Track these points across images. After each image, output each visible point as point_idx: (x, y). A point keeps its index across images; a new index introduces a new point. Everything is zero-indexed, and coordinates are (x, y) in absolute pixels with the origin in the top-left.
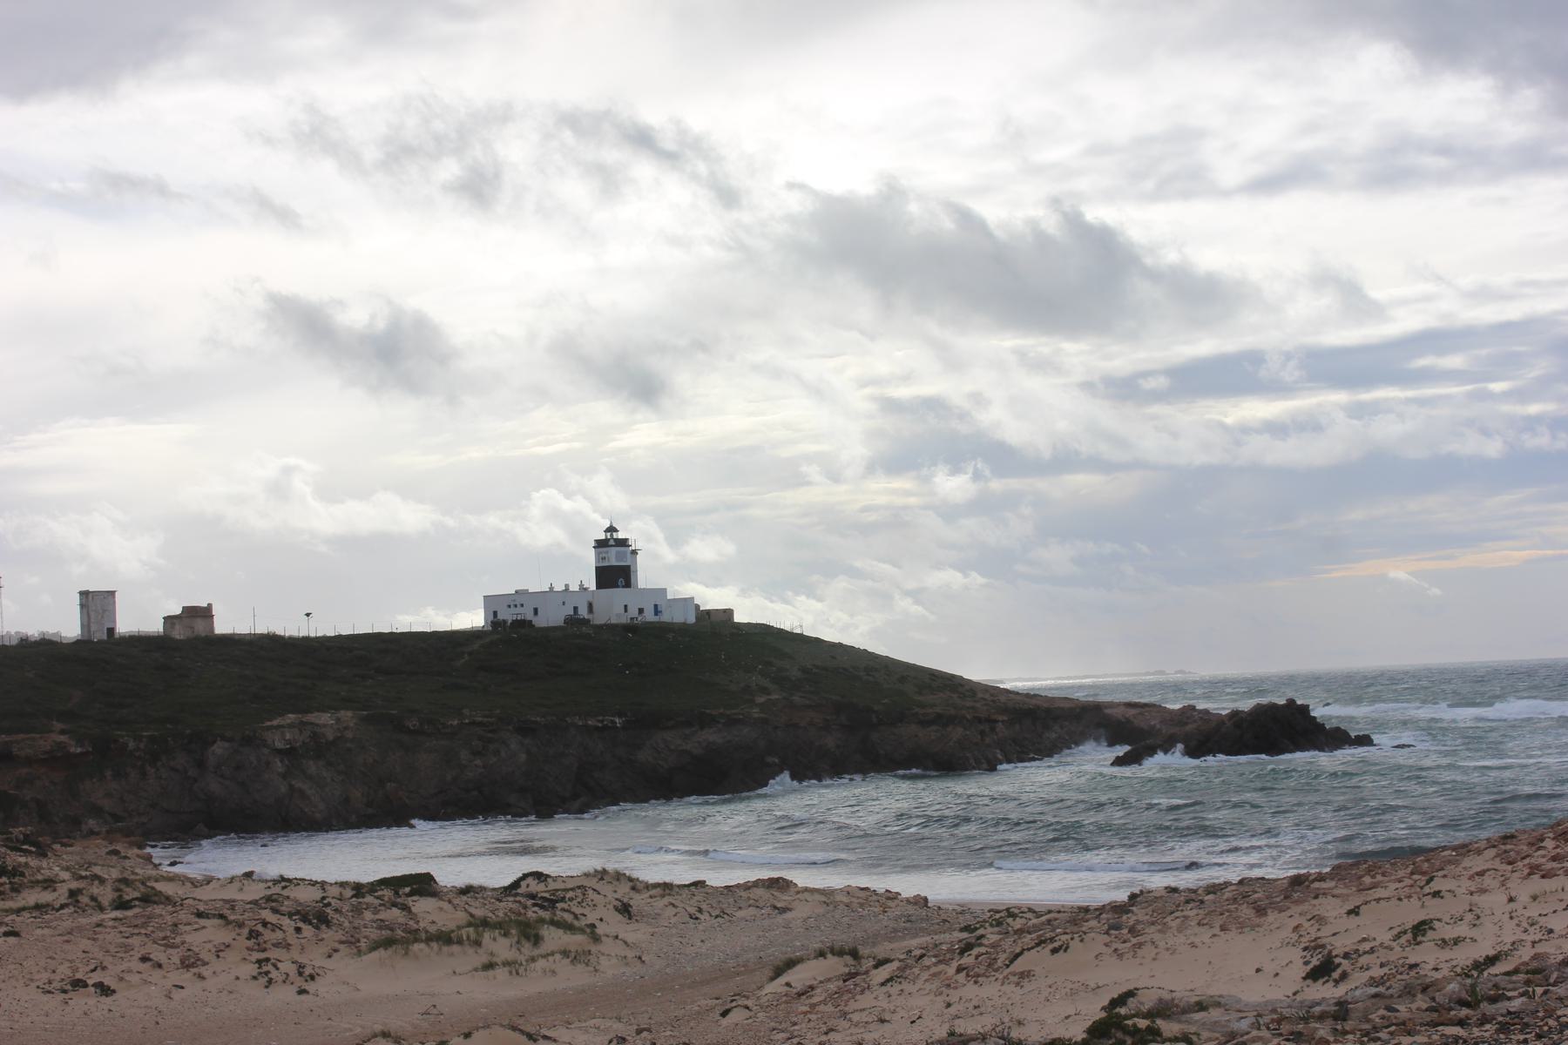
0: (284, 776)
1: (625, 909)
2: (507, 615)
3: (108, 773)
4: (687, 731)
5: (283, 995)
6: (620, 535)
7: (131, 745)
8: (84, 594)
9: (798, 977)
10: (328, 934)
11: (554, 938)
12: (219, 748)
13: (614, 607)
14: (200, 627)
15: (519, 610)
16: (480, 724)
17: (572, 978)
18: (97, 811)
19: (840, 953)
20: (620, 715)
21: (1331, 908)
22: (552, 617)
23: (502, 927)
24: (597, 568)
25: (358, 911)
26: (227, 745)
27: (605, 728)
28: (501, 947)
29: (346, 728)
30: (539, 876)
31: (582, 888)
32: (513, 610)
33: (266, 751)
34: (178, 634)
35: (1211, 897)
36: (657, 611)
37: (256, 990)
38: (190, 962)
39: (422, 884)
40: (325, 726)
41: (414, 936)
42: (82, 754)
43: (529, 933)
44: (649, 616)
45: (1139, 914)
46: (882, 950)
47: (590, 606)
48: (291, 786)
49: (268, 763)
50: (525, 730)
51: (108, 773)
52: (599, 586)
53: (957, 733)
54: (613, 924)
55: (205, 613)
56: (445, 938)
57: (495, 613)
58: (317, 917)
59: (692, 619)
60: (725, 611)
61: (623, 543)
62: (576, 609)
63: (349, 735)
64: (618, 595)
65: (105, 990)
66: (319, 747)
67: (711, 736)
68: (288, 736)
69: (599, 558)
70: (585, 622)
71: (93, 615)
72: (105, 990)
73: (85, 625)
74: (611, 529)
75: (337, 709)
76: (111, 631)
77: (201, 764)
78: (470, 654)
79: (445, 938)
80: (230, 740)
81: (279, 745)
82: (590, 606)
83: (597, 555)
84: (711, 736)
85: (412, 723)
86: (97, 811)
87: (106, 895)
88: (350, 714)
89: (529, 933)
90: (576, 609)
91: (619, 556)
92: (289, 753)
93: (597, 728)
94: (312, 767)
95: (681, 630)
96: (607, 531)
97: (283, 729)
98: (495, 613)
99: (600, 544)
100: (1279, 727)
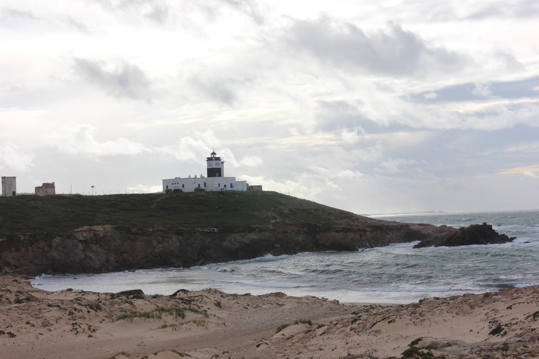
0: (83, 251)
1: (218, 304)
2: (172, 187)
3: (13, 249)
4: (243, 234)
5: (83, 337)
6: (217, 156)
7: (22, 238)
8: (3, 178)
9: (287, 332)
10: (101, 314)
11: (190, 316)
12: (57, 240)
13: (214, 184)
14: (49, 192)
15: (177, 185)
16: (161, 231)
17: (197, 331)
18: (8, 264)
19: (304, 322)
20: (217, 228)
21: (501, 306)
22: (190, 188)
23: (169, 311)
24: (208, 169)
25: (112, 304)
26: (60, 238)
27: (210, 232)
28: (169, 319)
29: (108, 232)
30: (184, 291)
31: (201, 296)
32: (174, 185)
33: (75, 240)
34: (41, 194)
35: (452, 301)
36: (231, 186)
37: (72, 335)
38: (45, 324)
39: (138, 294)
40: (99, 231)
41: (134, 314)
42: (3, 241)
43: (180, 314)
44: (228, 188)
45: (423, 308)
46: (320, 321)
47: (205, 184)
48: (86, 255)
49: (76, 246)
50: (179, 233)
51: (13, 249)
52: (209, 176)
53: (351, 235)
54: (214, 310)
55: (51, 186)
56: (147, 315)
57: (167, 187)
58: (96, 307)
59: (245, 189)
60: (259, 186)
61: (218, 159)
62: (199, 185)
63: (109, 235)
64: (216, 180)
65: (12, 335)
66: (97, 239)
67: (253, 236)
68: (84, 235)
69: (209, 165)
70: (203, 190)
71: (7, 186)
72: (12, 335)
73: (4, 191)
74: (214, 153)
75: (104, 224)
76: (14, 193)
77: (50, 246)
78: (157, 203)
79: (147, 315)
80: (61, 236)
81: (81, 238)
82: (205, 184)
83: (208, 164)
84: (253, 236)
85: (134, 230)
86: (8, 264)
87: (12, 298)
88: (109, 226)
89: (180, 314)
90: (199, 185)
91: (216, 164)
92: (85, 242)
93: (207, 232)
94: (94, 247)
95: (242, 193)
96: (212, 154)
97: (83, 232)
98: (167, 187)
99: (209, 159)
100: (480, 234)
